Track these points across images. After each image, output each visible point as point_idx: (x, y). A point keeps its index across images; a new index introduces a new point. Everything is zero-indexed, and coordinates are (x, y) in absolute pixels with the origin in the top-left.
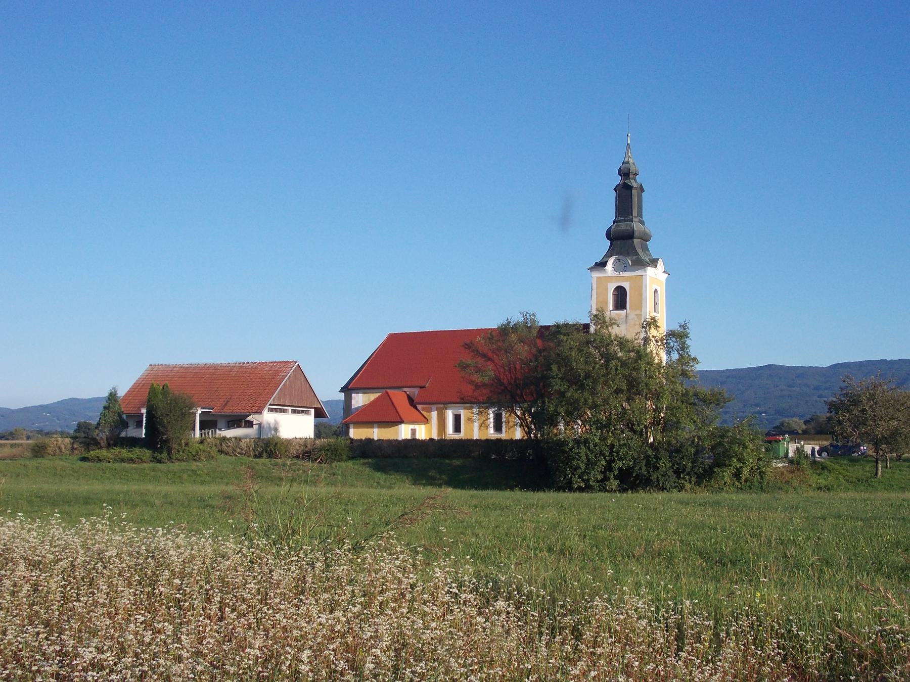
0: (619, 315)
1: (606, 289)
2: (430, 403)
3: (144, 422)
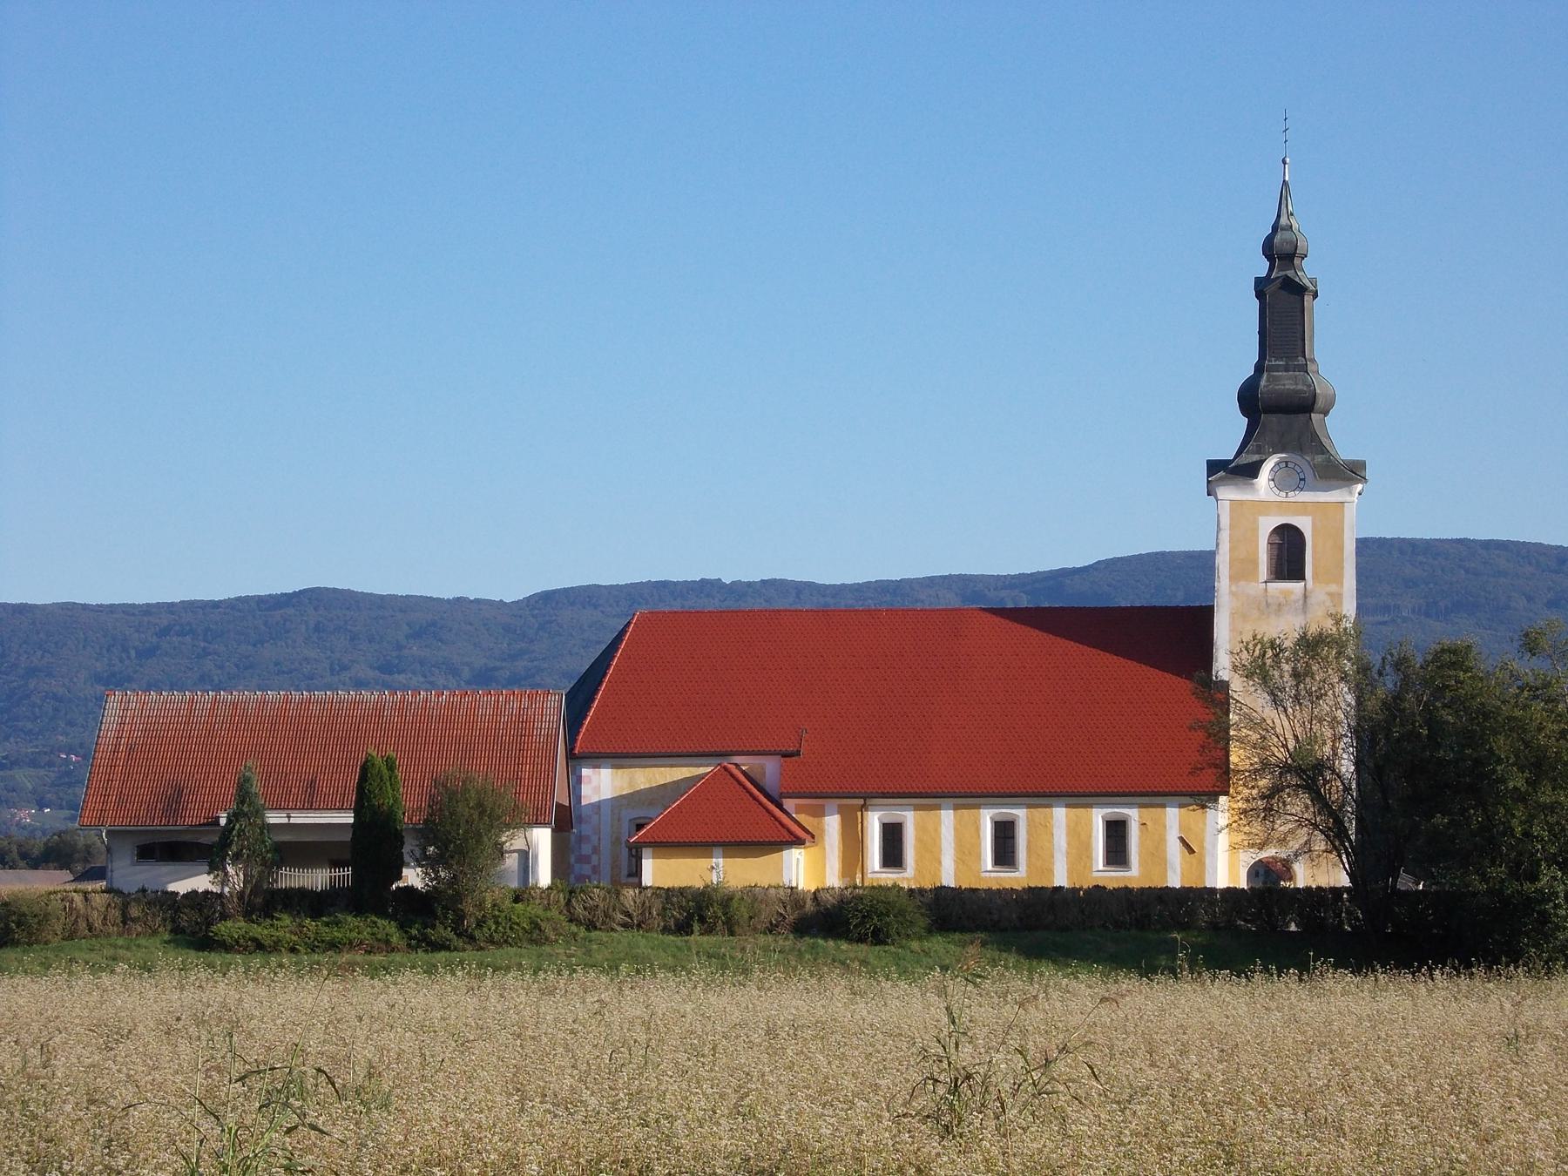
0: (1287, 593)
1: (1255, 530)
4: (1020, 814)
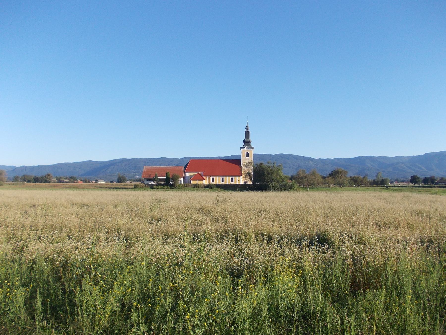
2: (207, 176)
3: (161, 177)
4: (224, 177)
